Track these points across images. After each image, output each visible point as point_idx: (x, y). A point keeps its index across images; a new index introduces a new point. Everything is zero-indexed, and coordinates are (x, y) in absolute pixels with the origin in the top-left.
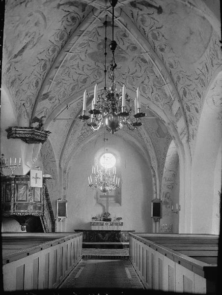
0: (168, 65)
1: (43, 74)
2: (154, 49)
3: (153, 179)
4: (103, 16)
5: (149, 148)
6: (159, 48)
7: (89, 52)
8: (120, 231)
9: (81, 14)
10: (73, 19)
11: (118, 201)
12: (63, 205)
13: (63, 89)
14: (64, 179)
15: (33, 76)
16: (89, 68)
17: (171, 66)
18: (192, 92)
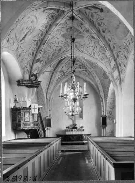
0: (108, 40)
1: (36, 48)
2: (99, 31)
3: (102, 103)
4: (69, 15)
5: (98, 85)
6: (102, 31)
7: (62, 33)
8: (82, 135)
9: (57, 14)
10: (52, 17)
11: (81, 116)
12: (49, 121)
13: (47, 55)
14: (49, 105)
16: (62, 42)
17: (109, 40)
18: (122, 55)
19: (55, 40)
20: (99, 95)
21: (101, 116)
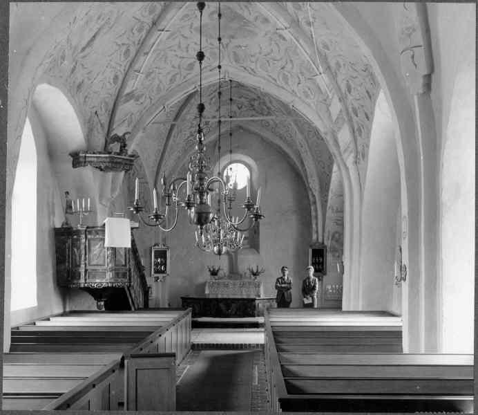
1: (125, 63)
3: (312, 208)
13: (157, 82)
15: (109, 70)
17: (326, 47)
19: (177, 41)
20: (307, 185)
21: (311, 246)
